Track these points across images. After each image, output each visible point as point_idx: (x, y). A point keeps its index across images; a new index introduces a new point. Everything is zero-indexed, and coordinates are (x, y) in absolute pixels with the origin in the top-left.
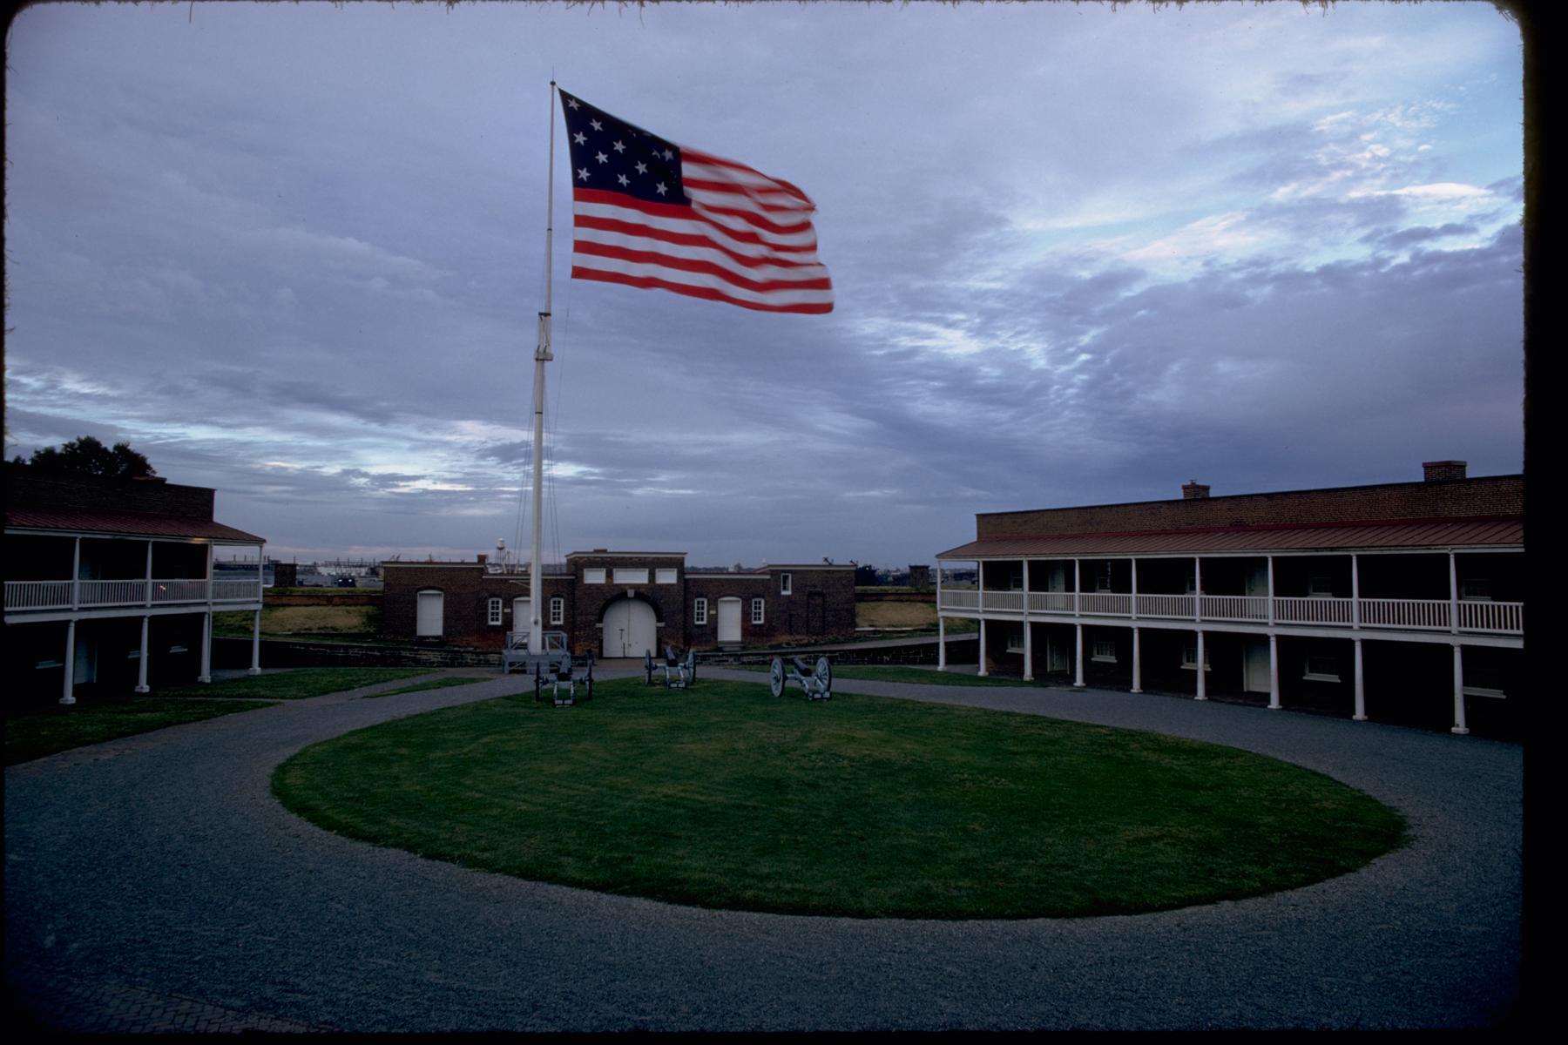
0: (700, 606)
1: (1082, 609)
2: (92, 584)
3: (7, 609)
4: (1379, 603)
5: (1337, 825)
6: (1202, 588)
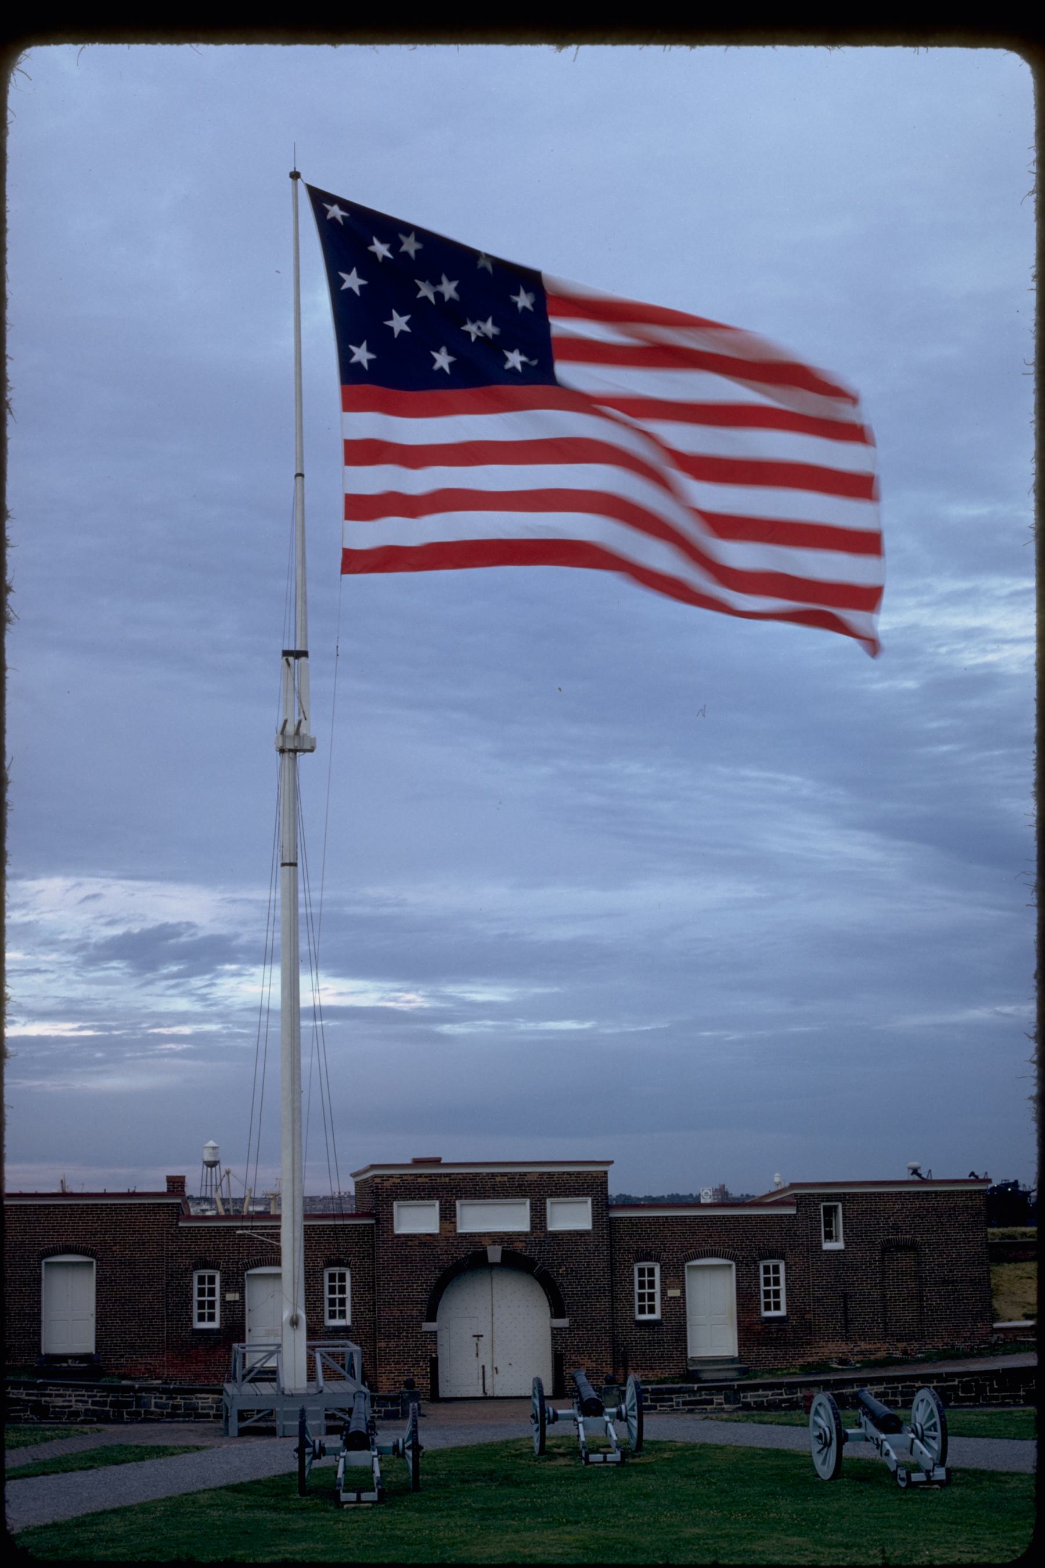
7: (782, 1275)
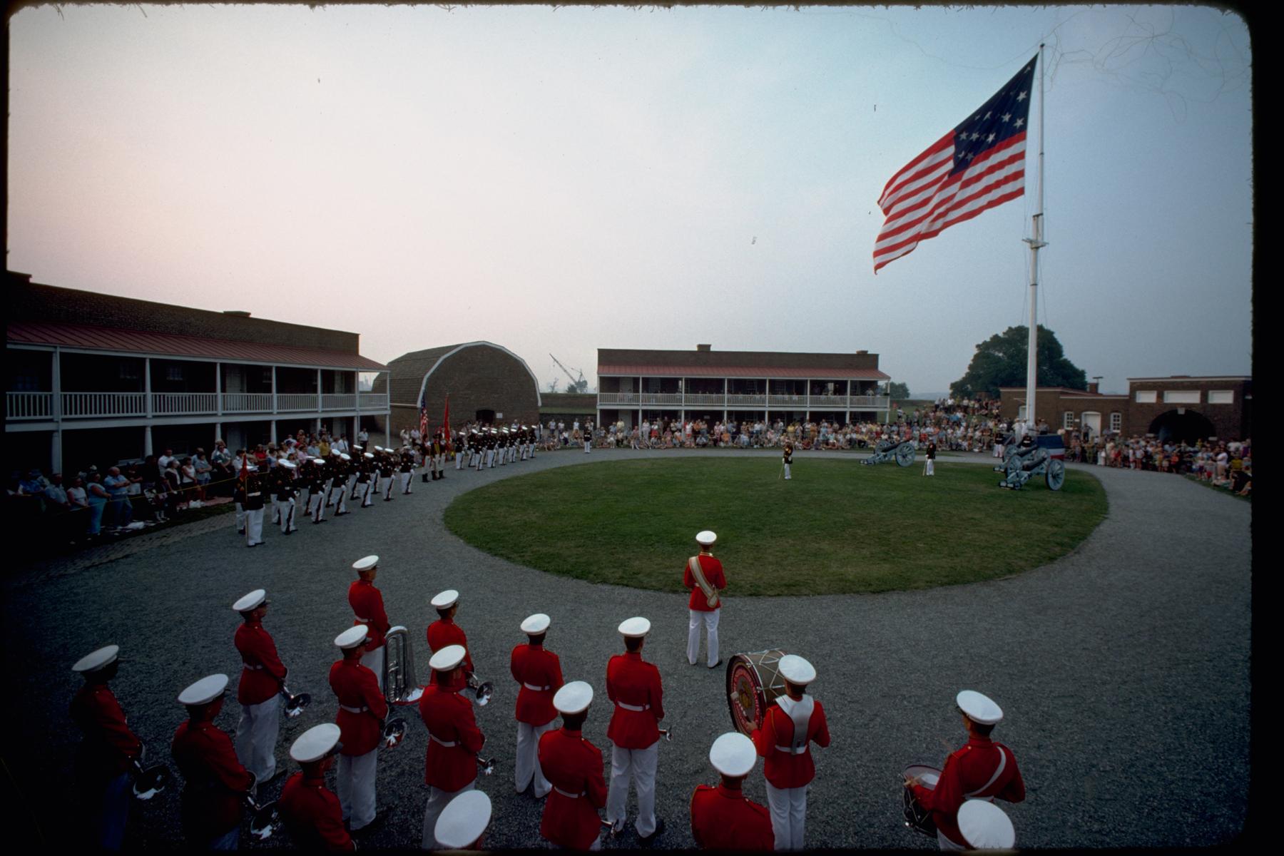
1: (769, 403)
2: (242, 396)
3: (8, 418)
4: (35, 397)
5: (410, 699)
6: (769, 391)
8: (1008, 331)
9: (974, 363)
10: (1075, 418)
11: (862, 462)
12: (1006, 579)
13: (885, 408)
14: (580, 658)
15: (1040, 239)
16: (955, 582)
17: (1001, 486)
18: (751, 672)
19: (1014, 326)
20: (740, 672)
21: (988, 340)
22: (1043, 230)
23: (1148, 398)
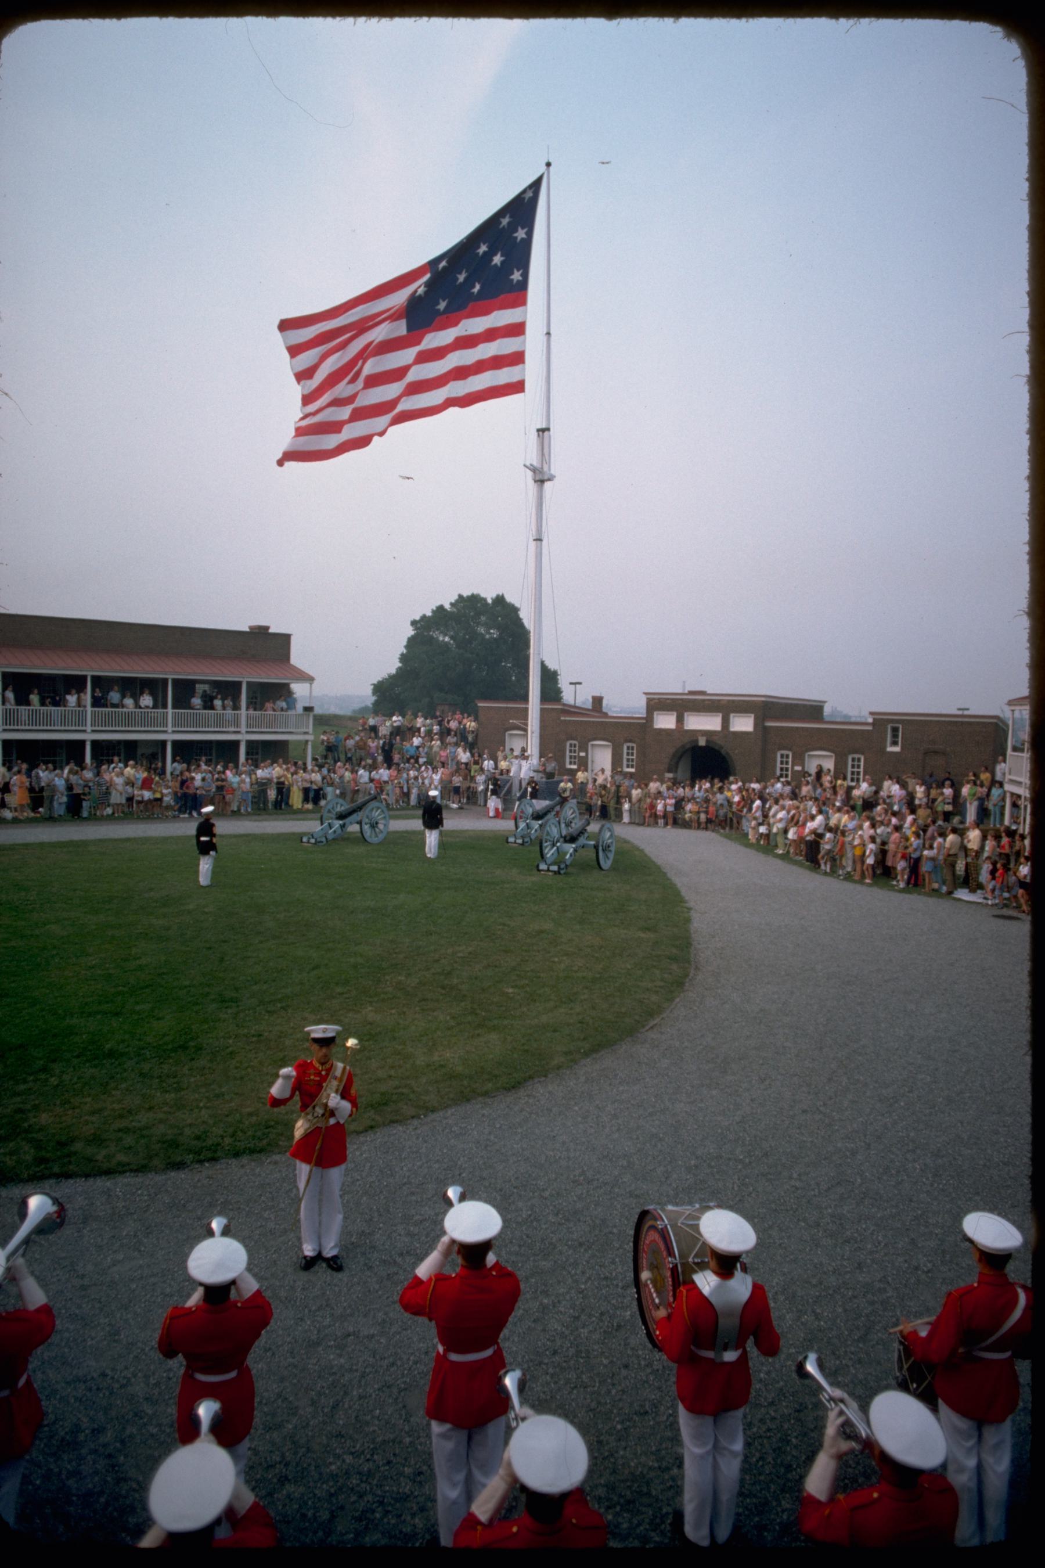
0: (856, 763)
1: (174, 725)
7: (862, 764)
8: (457, 601)
9: (408, 652)
10: (580, 750)
11: (305, 839)
12: (652, 1028)
13: (306, 733)
14: (104, 1375)
15: (546, 468)
16: (599, 1045)
17: (539, 870)
18: (664, 1234)
19: (466, 593)
20: (653, 1236)
21: (429, 614)
22: (550, 456)
23: (666, 722)
